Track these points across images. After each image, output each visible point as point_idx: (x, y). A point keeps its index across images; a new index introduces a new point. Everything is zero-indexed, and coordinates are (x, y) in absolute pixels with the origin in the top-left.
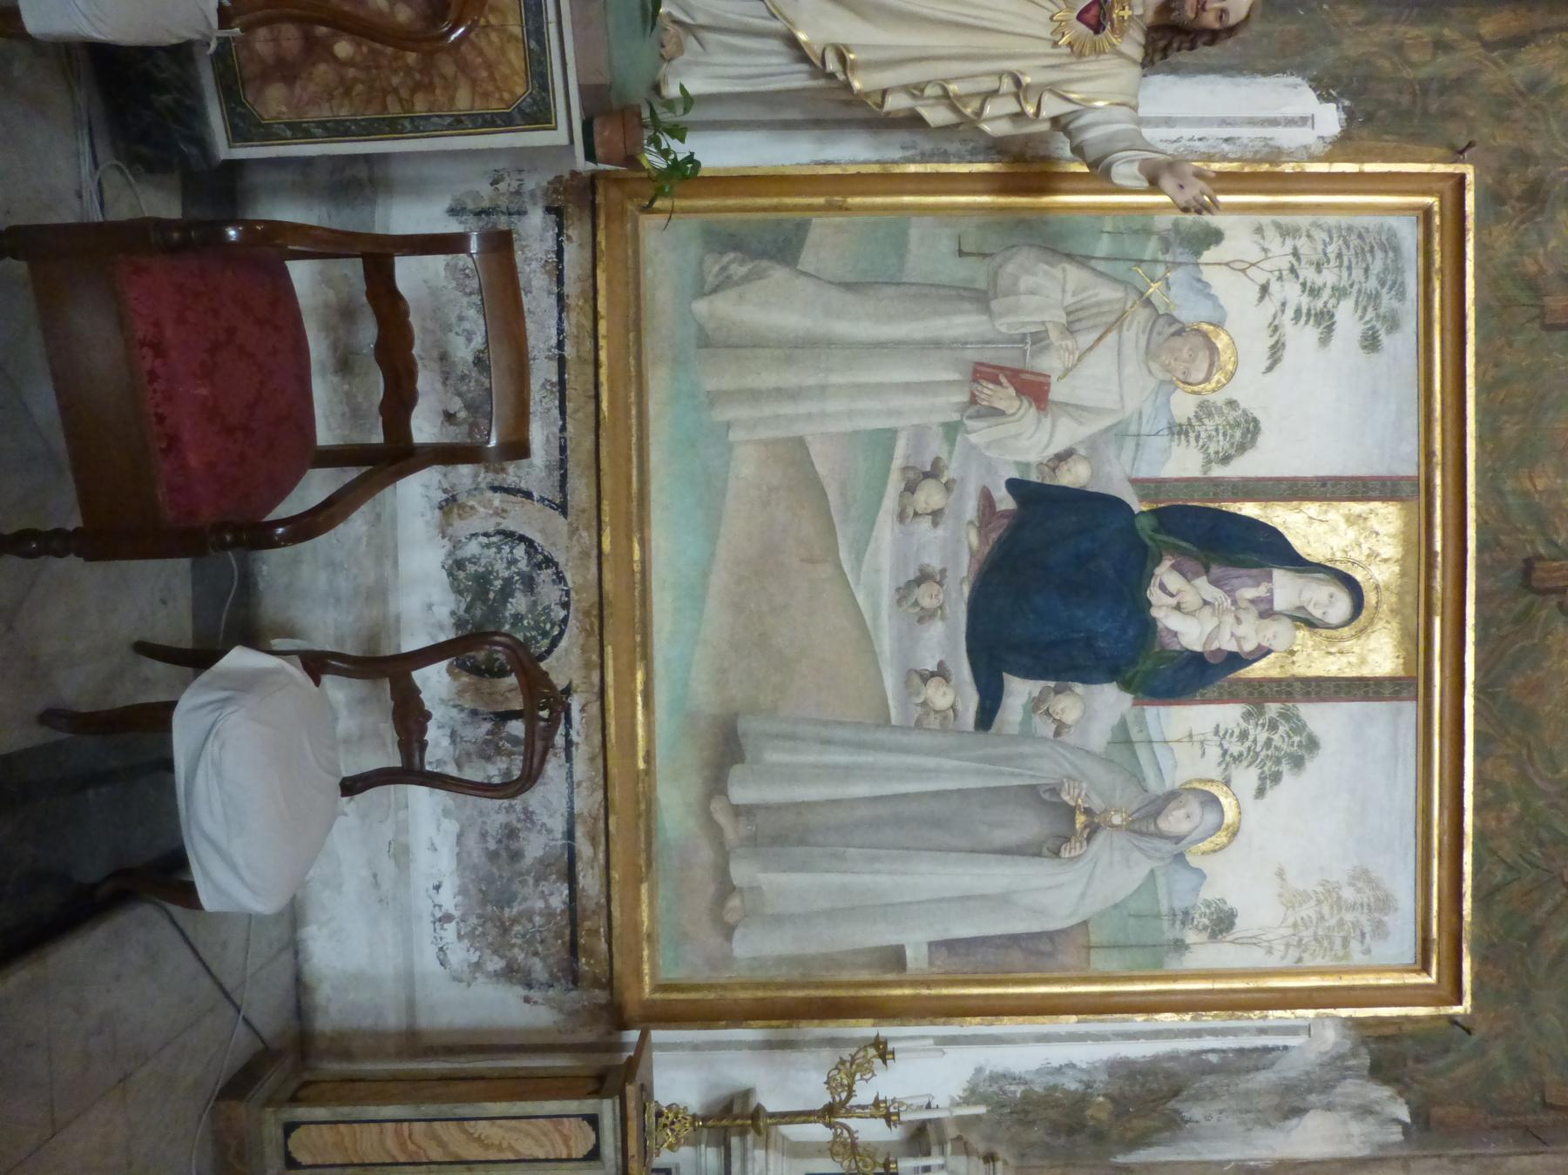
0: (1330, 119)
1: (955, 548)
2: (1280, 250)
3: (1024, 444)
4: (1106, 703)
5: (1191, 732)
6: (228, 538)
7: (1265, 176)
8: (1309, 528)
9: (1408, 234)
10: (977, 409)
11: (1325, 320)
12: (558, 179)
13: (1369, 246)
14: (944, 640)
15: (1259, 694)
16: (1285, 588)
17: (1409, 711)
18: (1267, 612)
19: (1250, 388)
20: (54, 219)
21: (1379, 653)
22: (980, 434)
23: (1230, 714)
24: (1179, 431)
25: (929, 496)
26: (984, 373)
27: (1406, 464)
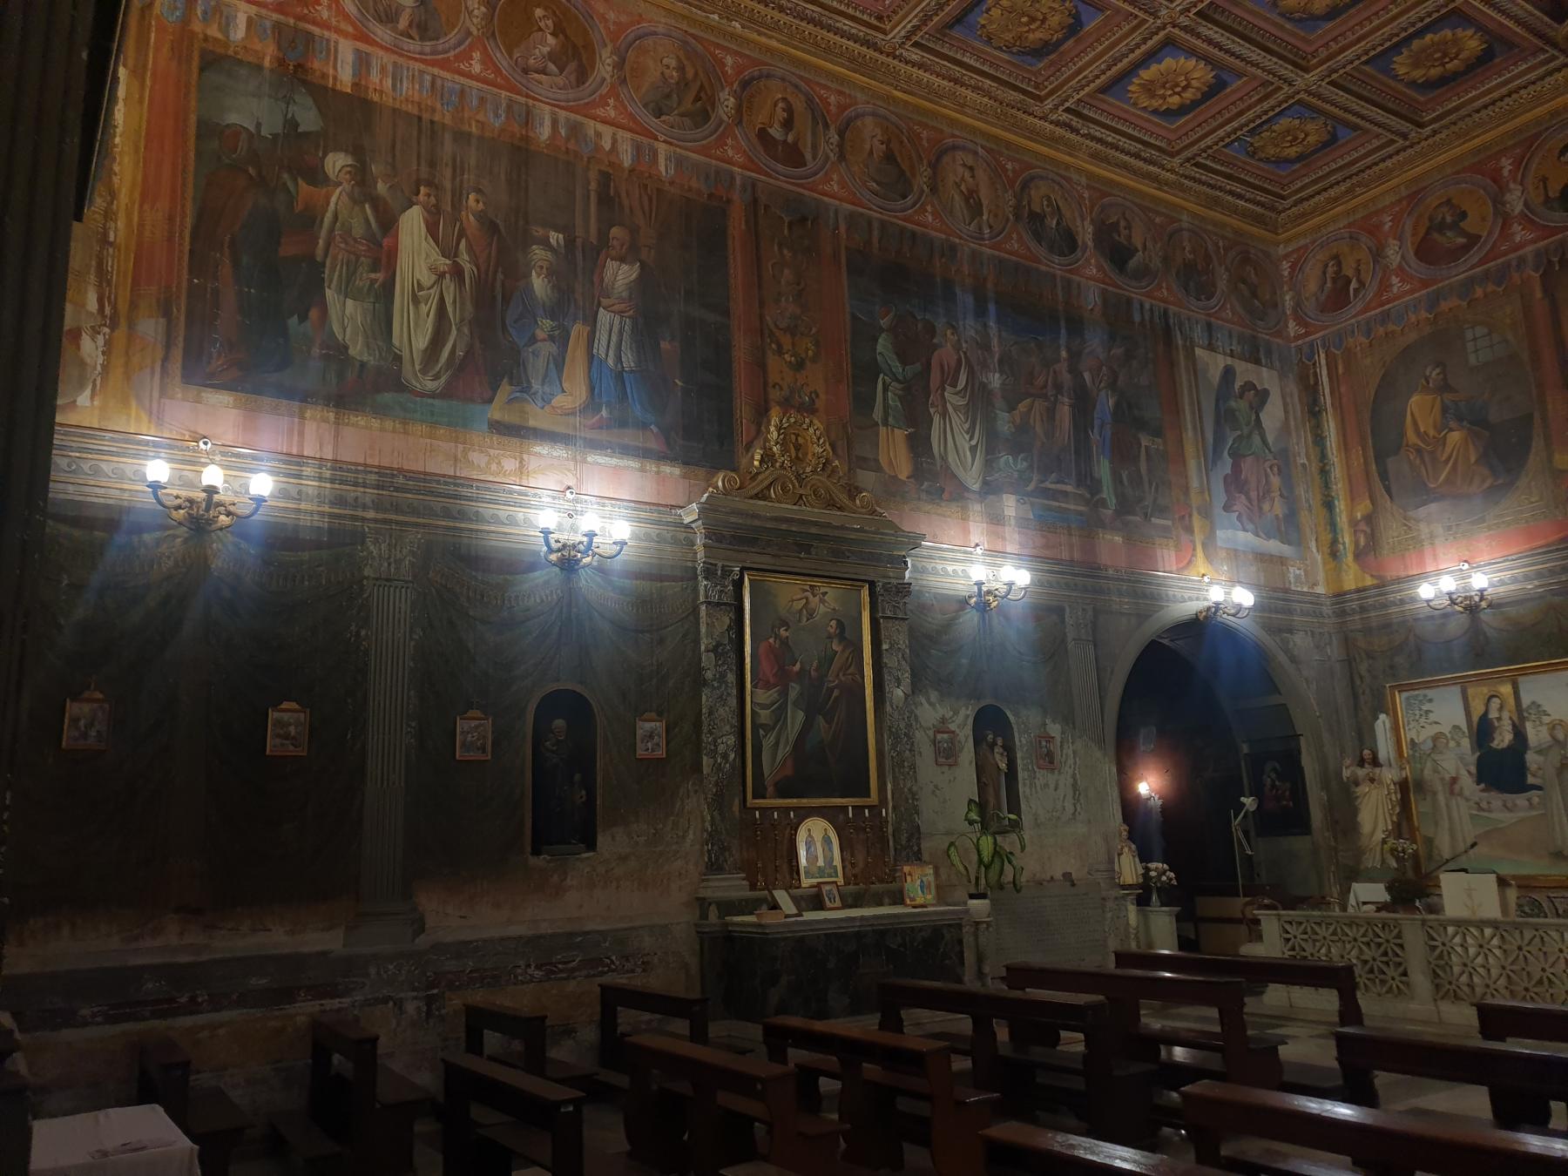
0: (1382, 717)
1: (1496, 799)
2: (1413, 724)
3: (1468, 783)
4: (1531, 758)
5: (1536, 734)
6: (759, 1087)
7: (1396, 728)
8: (1478, 709)
9: (1405, 695)
10: (1461, 794)
11: (1427, 712)
12: (1225, 478)
13: (1409, 705)
14: (1520, 800)
15: (1522, 719)
16: (1493, 715)
17: (1520, 679)
18: (1499, 719)
19: (1446, 730)
20: (1393, 1076)
21: (1506, 689)
22: (1467, 793)
23: (1529, 725)
24: (1458, 744)
25: (1484, 805)
26: (1452, 793)
27: (1457, 689)
